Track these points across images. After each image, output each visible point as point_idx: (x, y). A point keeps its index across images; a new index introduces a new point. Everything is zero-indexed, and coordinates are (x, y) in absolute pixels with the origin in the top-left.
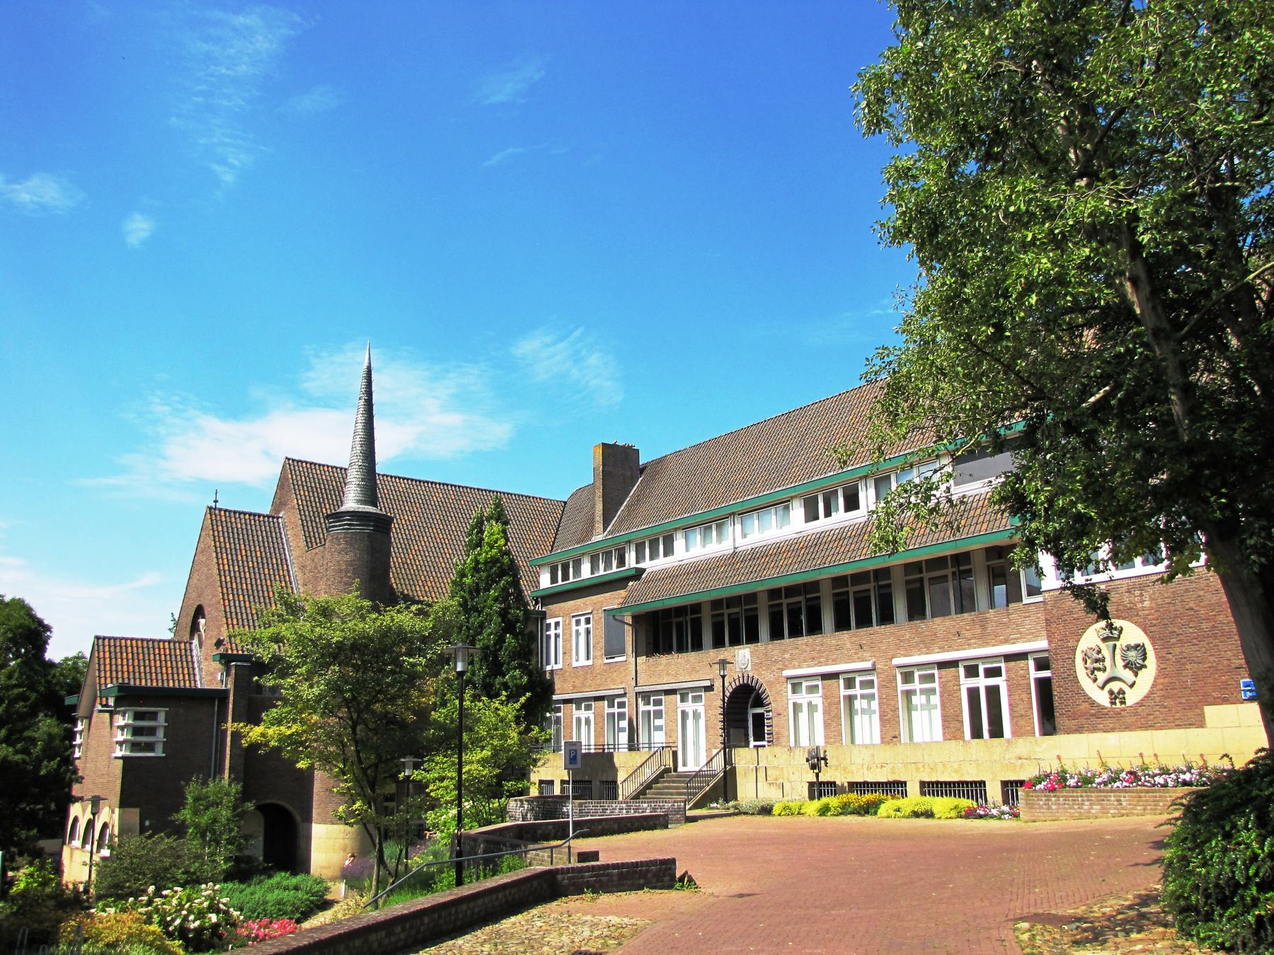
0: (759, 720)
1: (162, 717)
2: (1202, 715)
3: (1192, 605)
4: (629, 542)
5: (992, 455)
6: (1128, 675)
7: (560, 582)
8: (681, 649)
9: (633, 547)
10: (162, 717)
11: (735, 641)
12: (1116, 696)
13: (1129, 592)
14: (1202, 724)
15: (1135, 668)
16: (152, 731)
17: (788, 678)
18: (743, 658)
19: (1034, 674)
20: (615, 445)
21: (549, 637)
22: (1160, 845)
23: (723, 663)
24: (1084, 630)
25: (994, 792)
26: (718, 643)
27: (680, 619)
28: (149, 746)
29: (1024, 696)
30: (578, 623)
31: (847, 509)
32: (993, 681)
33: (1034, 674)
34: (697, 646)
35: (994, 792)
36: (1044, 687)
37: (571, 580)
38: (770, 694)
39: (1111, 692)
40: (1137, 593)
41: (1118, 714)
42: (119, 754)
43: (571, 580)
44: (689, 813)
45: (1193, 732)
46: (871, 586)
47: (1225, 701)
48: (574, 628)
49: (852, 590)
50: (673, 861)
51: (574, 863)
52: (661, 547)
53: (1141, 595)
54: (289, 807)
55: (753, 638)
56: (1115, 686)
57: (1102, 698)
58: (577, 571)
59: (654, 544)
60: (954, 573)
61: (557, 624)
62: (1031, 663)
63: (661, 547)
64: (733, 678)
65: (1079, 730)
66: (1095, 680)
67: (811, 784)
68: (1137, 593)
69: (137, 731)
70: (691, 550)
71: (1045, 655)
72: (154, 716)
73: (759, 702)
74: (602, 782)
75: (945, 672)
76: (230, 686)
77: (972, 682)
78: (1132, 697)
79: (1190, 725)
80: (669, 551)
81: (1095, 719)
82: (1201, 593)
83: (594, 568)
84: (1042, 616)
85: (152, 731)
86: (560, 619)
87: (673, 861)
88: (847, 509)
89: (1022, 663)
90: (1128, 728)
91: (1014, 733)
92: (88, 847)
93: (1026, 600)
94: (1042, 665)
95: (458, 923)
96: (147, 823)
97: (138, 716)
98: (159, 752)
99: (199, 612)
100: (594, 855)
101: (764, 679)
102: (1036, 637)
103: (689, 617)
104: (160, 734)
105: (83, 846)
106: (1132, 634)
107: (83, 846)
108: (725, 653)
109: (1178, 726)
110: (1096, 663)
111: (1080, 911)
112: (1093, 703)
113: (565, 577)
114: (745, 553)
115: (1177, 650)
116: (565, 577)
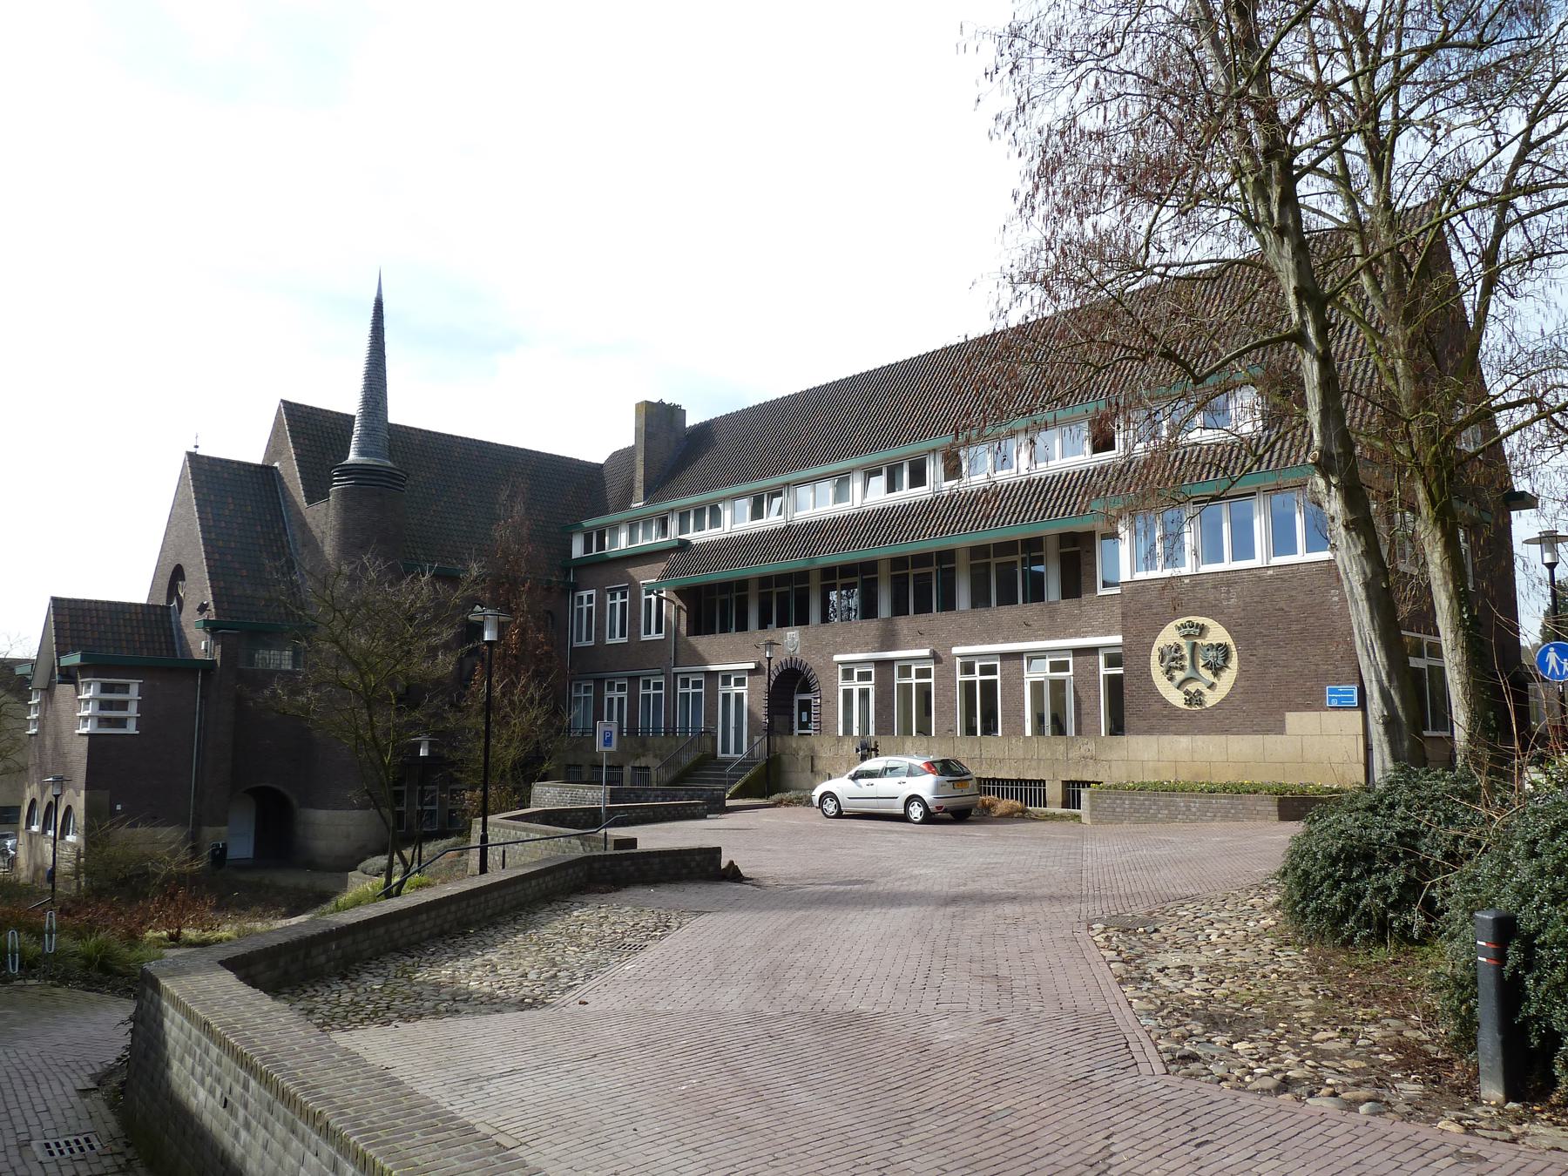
0: (806, 706)
2: (1283, 721)
3: (1282, 604)
4: (672, 510)
6: (1207, 675)
7: (594, 552)
8: (725, 629)
9: (677, 516)
11: (783, 623)
12: (1194, 699)
13: (1215, 587)
14: (1280, 729)
15: (1217, 670)
16: (123, 705)
17: (842, 663)
18: (792, 638)
19: (1104, 671)
20: (661, 404)
22: (1263, 889)
23: (771, 644)
24: (1163, 626)
25: (1054, 791)
26: (764, 624)
27: (725, 597)
28: (121, 723)
29: (1092, 693)
30: (613, 597)
31: (912, 485)
33: (1104, 671)
34: (742, 626)
35: (1054, 791)
36: (1115, 684)
38: (821, 678)
39: (1187, 693)
40: (1224, 589)
41: (1192, 716)
42: (84, 730)
43: (594, 552)
44: (729, 803)
45: (1271, 739)
46: (933, 569)
47: (1308, 707)
48: (609, 602)
49: (912, 572)
51: (611, 851)
52: (692, 520)
53: (1228, 592)
54: (282, 789)
55: (803, 620)
56: (1192, 687)
57: (1176, 698)
58: (614, 542)
59: (699, 513)
60: (1023, 560)
61: (590, 597)
62: (1102, 659)
63: (692, 520)
64: (779, 658)
65: (1150, 731)
66: (1171, 679)
68: (1224, 589)
69: (104, 705)
70: (736, 521)
71: (1119, 651)
72: (125, 689)
73: (806, 688)
74: (634, 768)
75: (1009, 663)
76: (218, 657)
78: (1211, 699)
79: (1267, 732)
80: (716, 521)
81: (1168, 721)
82: (1294, 593)
83: (632, 539)
84: (1118, 611)
85: (123, 705)
86: (593, 592)
88: (912, 485)
89: (1091, 659)
90: (1202, 732)
91: (1078, 732)
92: (51, 833)
93: (1101, 592)
94: (1113, 661)
95: (489, 912)
96: (119, 807)
97: (105, 688)
98: (131, 729)
99: (178, 574)
100: (632, 842)
101: (813, 661)
102: (1108, 633)
103: (734, 595)
104: (133, 710)
105: (44, 831)
106: (1218, 634)
107: (44, 831)
108: (773, 633)
109: (1256, 732)
110: (1172, 660)
112: (1166, 704)
114: (799, 527)
115: (1261, 652)
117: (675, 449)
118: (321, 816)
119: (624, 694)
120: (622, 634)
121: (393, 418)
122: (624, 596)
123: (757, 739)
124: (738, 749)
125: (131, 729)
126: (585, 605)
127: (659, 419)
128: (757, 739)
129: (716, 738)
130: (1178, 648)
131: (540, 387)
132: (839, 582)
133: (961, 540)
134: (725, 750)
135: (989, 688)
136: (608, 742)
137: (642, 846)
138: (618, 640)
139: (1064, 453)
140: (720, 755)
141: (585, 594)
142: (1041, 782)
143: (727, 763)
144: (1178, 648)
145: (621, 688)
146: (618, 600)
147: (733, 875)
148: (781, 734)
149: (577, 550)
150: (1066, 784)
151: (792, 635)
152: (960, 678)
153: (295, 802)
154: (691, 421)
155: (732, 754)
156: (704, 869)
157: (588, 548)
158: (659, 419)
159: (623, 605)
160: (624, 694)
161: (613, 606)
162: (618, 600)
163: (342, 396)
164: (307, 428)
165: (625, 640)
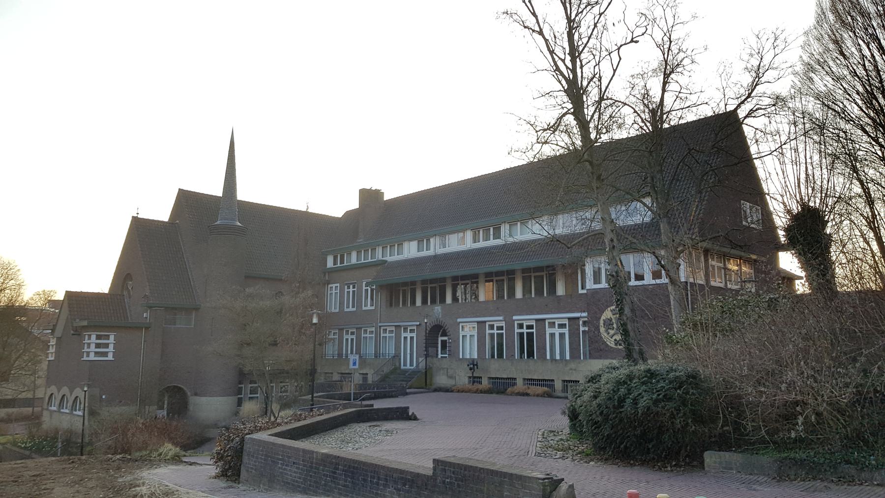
1: (112, 338)
5: (292, 487)
10: (112, 338)
16: (106, 346)
21: (331, 294)
25: (558, 385)
28: (105, 354)
30: (349, 288)
32: (562, 331)
35: (558, 385)
37: (345, 264)
43: (345, 264)
44: (408, 391)
48: (346, 290)
50: (408, 408)
54: (185, 389)
67: (470, 377)
70: (411, 250)
72: (108, 337)
77: (552, 330)
86: (338, 285)
87: (408, 408)
98: (110, 357)
104: (111, 347)
111: (167, 484)
113: (342, 262)
116: (342, 262)
117: (379, 215)
118: (203, 400)
119: (354, 337)
120: (353, 307)
121: (239, 198)
122: (354, 287)
123: (421, 359)
124: (411, 365)
125: (110, 357)
126: (334, 292)
127: (369, 197)
128: (421, 359)
129: (400, 359)
130: (611, 320)
131: (309, 175)
132: (460, 282)
133: (517, 265)
134: (405, 365)
135: (530, 335)
136: (354, 364)
137: (375, 407)
138: (351, 309)
139: (566, 224)
140: (402, 367)
141: (334, 286)
142: (553, 380)
143: (406, 371)
144: (611, 320)
145: (352, 333)
146: (351, 290)
147: (414, 418)
148: (432, 357)
149: (330, 263)
150: (564, 381)
151: (438, 309)
152: (517, 331)
153: (189, 394)
154: (386, 198)
155: (408, 367)
156: (403, 415)
157: (335, 263)
158: (369, 197)
159: (354, 292)
160: (354, 337)
161: (349, 292)
162: (351, 290)
163: (212, 186)
164: (187, 201)
165: (354, 309)
